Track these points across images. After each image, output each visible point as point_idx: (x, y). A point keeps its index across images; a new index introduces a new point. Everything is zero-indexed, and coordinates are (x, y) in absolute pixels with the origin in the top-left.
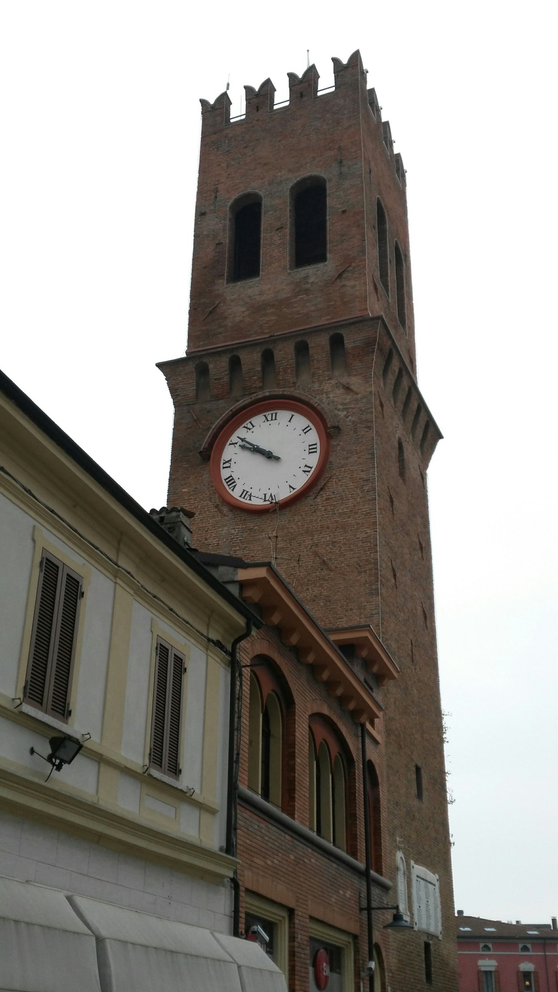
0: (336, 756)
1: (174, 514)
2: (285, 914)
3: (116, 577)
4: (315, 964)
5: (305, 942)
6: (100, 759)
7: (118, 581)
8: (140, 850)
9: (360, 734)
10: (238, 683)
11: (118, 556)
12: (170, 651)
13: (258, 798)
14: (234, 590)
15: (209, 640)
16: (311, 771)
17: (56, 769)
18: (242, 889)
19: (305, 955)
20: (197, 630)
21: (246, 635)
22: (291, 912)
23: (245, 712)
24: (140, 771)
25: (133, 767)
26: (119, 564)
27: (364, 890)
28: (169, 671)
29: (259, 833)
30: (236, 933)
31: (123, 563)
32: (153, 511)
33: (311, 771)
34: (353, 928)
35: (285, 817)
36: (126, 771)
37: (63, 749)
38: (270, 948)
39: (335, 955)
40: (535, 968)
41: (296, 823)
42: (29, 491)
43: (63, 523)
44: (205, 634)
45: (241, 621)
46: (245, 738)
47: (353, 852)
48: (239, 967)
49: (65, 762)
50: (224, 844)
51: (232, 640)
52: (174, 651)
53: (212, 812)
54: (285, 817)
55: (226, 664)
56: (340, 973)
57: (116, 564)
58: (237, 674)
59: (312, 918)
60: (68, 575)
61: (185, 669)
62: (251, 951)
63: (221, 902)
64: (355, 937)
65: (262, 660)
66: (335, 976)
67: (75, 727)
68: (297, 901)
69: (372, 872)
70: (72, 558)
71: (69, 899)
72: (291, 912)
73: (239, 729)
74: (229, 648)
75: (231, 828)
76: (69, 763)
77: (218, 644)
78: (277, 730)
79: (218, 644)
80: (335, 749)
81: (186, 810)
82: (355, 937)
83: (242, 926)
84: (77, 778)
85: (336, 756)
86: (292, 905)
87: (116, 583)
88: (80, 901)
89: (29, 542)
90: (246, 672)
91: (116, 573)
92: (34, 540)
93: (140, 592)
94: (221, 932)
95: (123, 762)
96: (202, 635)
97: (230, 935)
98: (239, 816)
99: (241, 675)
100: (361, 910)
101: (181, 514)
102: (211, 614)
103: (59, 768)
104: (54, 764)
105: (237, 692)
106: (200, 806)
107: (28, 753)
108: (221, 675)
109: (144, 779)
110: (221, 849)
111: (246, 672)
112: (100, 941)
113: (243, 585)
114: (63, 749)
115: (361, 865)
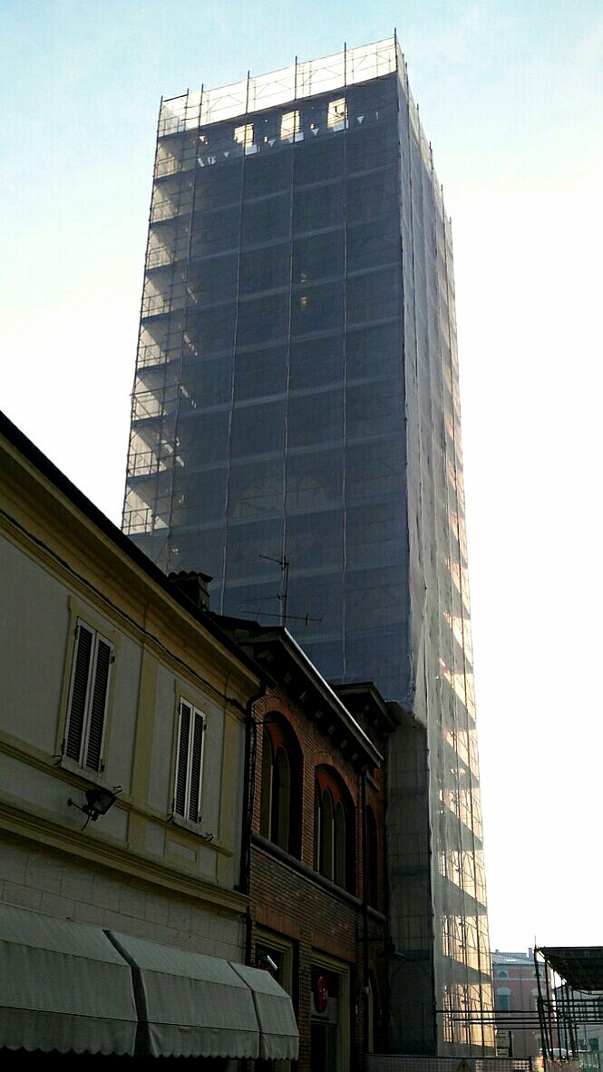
0: (339, 803)
1: (192, 578)
2: (290, 945)
3: (143, 642)
4: (315, 989)
5: (308, 970)
6: (129, 808)
7: (145, 645)
8: (175, 892)
9: (360, 782)
10: (252, 739)
11: (145, 622)
12: (93, 636)
13: (268, 841)
14: (249, 652)
15: (227, 700)
16: (316, 815)
17: (92, 819)
18: (254, 923)
19: (306, 981)
20: (9, 518)
21: (261, 693)
22: (296, 943)
23: (258, 765)
24: (51, 763)
25: (158, 816)
26: (146, 630)
27: (361, 922)
28: (189, 728)
29: (268, 873)
30: (248, 963)
31: (150, 629)
32: (172, 575)
33: (316, 815)
34: (350, 956)
35: (290, 857)
36: (153, 819)
37: (99, 799)
38: (277, 975)
39: (332, 981)
40: (512, 993)
41: (302, 864)
42: (65, 564)
43: (52, 556)
44: (223, 694)
45: (256, 681)
46: (258, 788)
47: (351, 887)
48: (253, 992)
49: (100, 813)
50: (237, 883)
51: (248, 699)
52: (100, 637)
53: (229, 855)
54: (290, 857)
55: (241, 720)
56: (337, 997)
57: (144, 631)
58: (252, 730)
59: (314, 949)
60: (100, 641)
61: (113, 658)
62: (262, 980)
63: (232, 933)
64: (350, 964)
65: (273, 717)
66: (333, 1000)
67: (107, 781)
68: (301, 933)
69: (369, 907)
70: (104, 628)
71: (107, 933)
72: (296, 943)
73: (253, 780)
74: (244, 706)
75: (245, 870)
76: (104, 813)
77: (234, 703)
78: (286, 778)
79: (234, 703)
80: (337, 798)
81: (204, 852)
82: (350, 964)
83: (253, 956)
84: (110, 825)
85: (325, 791)
86: (297, 936)
87: (143, 648)
88: (116, 935)
89: (65, 613)
90: (260, 728)
91: (144, 637)
92: (69, 609)
93: (166, 656)
94: (235, 962)
95: (151, 813)
96: (221, 694)
97: (242, 963)
98: (251, 859)
99: (255, 731)
100: (357, 940)
101: (200, 579)
102: (227, 672)
103: (95, 818)
104: (90, 815)
105: (251, 746)
106: (217, 849)
107: (66, 803)
108: (236, 729)
109: (170, 825)
110: (235, 888)
111: (260, 728)
112: (253, 992)
113: (259, 648)
114: (99, 799)
115: (359, 901)
